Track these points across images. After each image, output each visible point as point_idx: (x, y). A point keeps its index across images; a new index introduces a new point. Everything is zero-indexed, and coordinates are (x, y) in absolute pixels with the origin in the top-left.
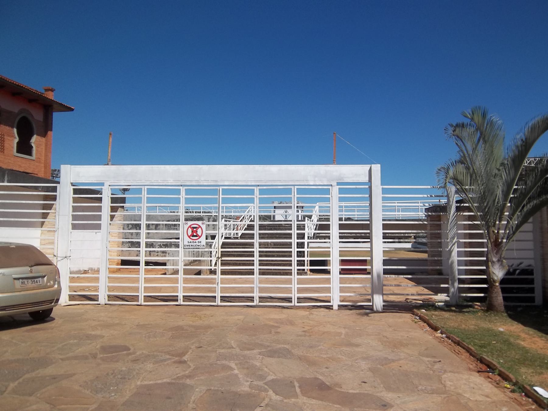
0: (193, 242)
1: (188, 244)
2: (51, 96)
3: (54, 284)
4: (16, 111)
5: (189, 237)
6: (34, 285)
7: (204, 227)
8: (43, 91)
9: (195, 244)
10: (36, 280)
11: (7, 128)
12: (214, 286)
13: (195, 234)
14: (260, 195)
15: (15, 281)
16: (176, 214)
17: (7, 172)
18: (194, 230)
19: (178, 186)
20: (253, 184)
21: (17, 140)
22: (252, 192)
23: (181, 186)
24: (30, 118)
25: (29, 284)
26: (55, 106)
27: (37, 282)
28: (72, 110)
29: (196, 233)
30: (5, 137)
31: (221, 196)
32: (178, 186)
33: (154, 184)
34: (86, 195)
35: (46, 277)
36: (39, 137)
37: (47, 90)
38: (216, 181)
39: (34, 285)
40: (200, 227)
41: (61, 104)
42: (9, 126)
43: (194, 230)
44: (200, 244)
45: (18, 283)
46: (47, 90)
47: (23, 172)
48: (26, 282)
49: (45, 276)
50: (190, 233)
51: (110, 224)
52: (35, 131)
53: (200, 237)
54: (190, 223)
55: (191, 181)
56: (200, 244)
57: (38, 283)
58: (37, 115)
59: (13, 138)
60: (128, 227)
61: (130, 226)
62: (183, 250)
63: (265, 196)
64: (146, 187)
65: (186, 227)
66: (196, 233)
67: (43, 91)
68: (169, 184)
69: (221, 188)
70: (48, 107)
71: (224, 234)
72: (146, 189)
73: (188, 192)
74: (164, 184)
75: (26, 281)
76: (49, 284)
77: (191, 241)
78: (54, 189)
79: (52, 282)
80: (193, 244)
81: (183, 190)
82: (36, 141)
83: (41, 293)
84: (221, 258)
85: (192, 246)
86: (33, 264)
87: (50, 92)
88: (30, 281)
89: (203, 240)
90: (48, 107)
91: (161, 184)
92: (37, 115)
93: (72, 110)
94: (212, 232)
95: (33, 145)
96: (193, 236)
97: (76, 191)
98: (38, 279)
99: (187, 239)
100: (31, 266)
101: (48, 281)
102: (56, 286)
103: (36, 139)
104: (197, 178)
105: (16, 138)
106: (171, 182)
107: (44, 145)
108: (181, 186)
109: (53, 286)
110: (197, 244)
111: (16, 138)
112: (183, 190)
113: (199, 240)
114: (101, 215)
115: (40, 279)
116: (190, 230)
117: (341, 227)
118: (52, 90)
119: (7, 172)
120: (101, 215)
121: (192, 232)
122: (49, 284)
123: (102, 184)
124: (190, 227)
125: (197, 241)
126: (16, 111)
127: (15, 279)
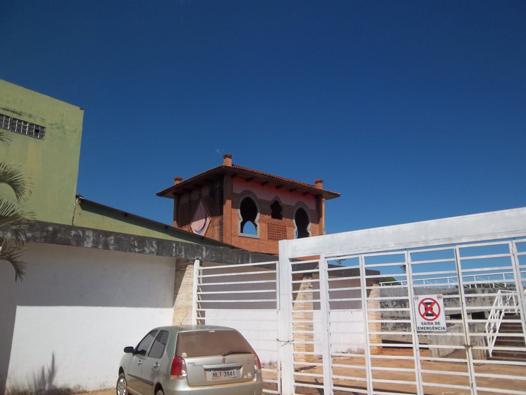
0: (429, 324)
1: (422, 326)
2: (320, 187)
3: (253, 377)
4: (294, 204)
5: (423, 316)
6: (227, 378)
7: (441, 302)
8: (314, 184)
9: (431, 326)
10: (230, 371)
11: (288, 219)
12: (467, 388)
13: (430, 312)
14: (518, 251)
15: (208, 372)
16: (402, 286)
17: (251, 254)
18: (428, 306)
19: (402, 250)
20: (505, 236)
21: (296, 229)
22: (505, 249)
23: (405, 249)
24: (305, 209)
25: (222, 376)
26: (324, 195)
27: (231, 375)
28: (339, 196)
29: (432, 311)
30: (287, 228)
31: (459, 258)
32: (402, 250)
33: (373, 251)
34: (304, 269)
35: (242, 369)
36: (314, 224)
37: (316, 182)
38: (450, 239)
39: (227, 378)
40: (435, 302)
41: (329, 192)
42: (289, 218)
43: (428, 306)
44: (438, 326)
45: (210, 374)
46: (316, 182)
47: (267, 254)
48: (218, 374)
49: (240, 367)
50: (423, 311)
51: (293, 304)
52: (259, 210)
53: (437, 316)
54: (422, 297)
55: (416, 242)
56: (438, 326)
57: (233, 376)
58: (310, 205)
59: (292, 228)
60: (392, 304)
61: (395, 303)
62: (417, 334)
63: (232, 283)
64: (363, 256)
65: (417, 303)
66: (432, 311)
67: (314, 184)
68: (390, 249)
69: (457, 247)
70: (318, 196)
71: (503, 310)
72: (363, 258)
73: (414, 257)
74: (384, 250)
75: (218, 372)
76: (245, 377)
77: (426, 321)
78: (273, 267)
79: (250, 375)
80: (429, 326)
81: (407, 254)
82: (311, 228)
83: (235, 388)
84: (471, 346)
85: (427, 328)
86: (227, 353)
87: (319, 183)
88: (223, 372)
89: (442, 320)
90: (318, 196)
91: (381, 250)
92: (310, 205)
93: (339, 196)
94: (454, 309)
95: (309, 232)
96: (428, 315)
97: (294, 268)
98: (232, 371)
99: (420, 320)
100: (225, 355)
101: (245, 373)
102: (255, 380)
103: (311, 226)
104: (423, 238)
105: (294, 227)
106: (392, 246)
107: (318, 231)
108: (405, 249)
109: (251, 380)
110: (435, 326)
111: (294, 227)
112: (407, 254)
113: (437, 320)
114: (319, 292)
115: (235, 370)
116: (423, 307)
117: (331, 274)
118: (321, 182)
119: (251, 254)
120: (319, 292)
121: (426, 309)
122: (245, 377)
123: (318, 257)
124: (422, 302)
125: (434, 322)
126: (294, 204)
127: (206, 370)
